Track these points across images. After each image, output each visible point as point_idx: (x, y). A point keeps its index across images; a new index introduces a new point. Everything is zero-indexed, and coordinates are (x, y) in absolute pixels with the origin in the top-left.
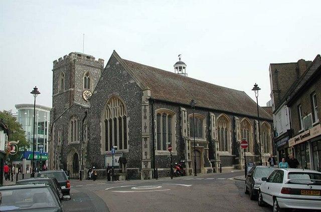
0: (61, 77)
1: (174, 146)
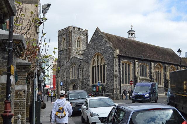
0: (63, 40)
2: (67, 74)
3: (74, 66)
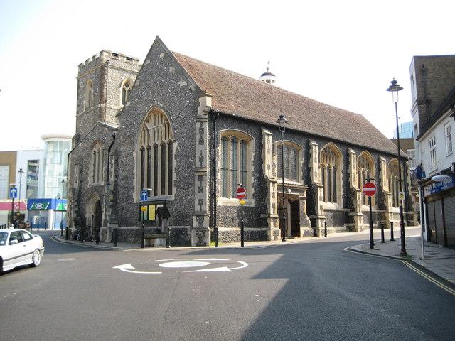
0: (88, 88)
1: (251, 190)
2: (81, 171)
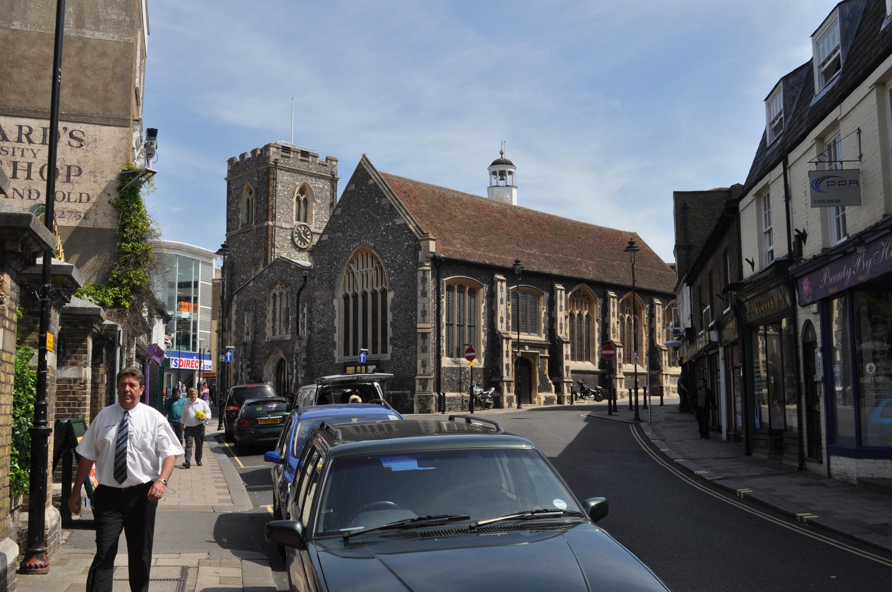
0: (245, 195)
2: (255, 320)
3: (281, 293)
